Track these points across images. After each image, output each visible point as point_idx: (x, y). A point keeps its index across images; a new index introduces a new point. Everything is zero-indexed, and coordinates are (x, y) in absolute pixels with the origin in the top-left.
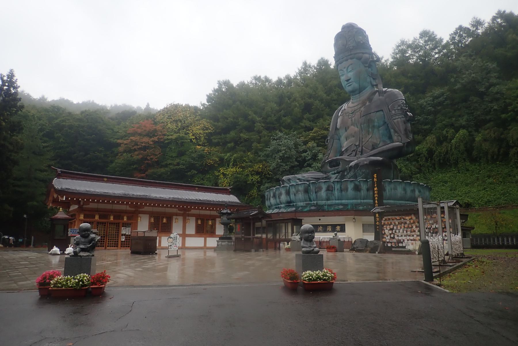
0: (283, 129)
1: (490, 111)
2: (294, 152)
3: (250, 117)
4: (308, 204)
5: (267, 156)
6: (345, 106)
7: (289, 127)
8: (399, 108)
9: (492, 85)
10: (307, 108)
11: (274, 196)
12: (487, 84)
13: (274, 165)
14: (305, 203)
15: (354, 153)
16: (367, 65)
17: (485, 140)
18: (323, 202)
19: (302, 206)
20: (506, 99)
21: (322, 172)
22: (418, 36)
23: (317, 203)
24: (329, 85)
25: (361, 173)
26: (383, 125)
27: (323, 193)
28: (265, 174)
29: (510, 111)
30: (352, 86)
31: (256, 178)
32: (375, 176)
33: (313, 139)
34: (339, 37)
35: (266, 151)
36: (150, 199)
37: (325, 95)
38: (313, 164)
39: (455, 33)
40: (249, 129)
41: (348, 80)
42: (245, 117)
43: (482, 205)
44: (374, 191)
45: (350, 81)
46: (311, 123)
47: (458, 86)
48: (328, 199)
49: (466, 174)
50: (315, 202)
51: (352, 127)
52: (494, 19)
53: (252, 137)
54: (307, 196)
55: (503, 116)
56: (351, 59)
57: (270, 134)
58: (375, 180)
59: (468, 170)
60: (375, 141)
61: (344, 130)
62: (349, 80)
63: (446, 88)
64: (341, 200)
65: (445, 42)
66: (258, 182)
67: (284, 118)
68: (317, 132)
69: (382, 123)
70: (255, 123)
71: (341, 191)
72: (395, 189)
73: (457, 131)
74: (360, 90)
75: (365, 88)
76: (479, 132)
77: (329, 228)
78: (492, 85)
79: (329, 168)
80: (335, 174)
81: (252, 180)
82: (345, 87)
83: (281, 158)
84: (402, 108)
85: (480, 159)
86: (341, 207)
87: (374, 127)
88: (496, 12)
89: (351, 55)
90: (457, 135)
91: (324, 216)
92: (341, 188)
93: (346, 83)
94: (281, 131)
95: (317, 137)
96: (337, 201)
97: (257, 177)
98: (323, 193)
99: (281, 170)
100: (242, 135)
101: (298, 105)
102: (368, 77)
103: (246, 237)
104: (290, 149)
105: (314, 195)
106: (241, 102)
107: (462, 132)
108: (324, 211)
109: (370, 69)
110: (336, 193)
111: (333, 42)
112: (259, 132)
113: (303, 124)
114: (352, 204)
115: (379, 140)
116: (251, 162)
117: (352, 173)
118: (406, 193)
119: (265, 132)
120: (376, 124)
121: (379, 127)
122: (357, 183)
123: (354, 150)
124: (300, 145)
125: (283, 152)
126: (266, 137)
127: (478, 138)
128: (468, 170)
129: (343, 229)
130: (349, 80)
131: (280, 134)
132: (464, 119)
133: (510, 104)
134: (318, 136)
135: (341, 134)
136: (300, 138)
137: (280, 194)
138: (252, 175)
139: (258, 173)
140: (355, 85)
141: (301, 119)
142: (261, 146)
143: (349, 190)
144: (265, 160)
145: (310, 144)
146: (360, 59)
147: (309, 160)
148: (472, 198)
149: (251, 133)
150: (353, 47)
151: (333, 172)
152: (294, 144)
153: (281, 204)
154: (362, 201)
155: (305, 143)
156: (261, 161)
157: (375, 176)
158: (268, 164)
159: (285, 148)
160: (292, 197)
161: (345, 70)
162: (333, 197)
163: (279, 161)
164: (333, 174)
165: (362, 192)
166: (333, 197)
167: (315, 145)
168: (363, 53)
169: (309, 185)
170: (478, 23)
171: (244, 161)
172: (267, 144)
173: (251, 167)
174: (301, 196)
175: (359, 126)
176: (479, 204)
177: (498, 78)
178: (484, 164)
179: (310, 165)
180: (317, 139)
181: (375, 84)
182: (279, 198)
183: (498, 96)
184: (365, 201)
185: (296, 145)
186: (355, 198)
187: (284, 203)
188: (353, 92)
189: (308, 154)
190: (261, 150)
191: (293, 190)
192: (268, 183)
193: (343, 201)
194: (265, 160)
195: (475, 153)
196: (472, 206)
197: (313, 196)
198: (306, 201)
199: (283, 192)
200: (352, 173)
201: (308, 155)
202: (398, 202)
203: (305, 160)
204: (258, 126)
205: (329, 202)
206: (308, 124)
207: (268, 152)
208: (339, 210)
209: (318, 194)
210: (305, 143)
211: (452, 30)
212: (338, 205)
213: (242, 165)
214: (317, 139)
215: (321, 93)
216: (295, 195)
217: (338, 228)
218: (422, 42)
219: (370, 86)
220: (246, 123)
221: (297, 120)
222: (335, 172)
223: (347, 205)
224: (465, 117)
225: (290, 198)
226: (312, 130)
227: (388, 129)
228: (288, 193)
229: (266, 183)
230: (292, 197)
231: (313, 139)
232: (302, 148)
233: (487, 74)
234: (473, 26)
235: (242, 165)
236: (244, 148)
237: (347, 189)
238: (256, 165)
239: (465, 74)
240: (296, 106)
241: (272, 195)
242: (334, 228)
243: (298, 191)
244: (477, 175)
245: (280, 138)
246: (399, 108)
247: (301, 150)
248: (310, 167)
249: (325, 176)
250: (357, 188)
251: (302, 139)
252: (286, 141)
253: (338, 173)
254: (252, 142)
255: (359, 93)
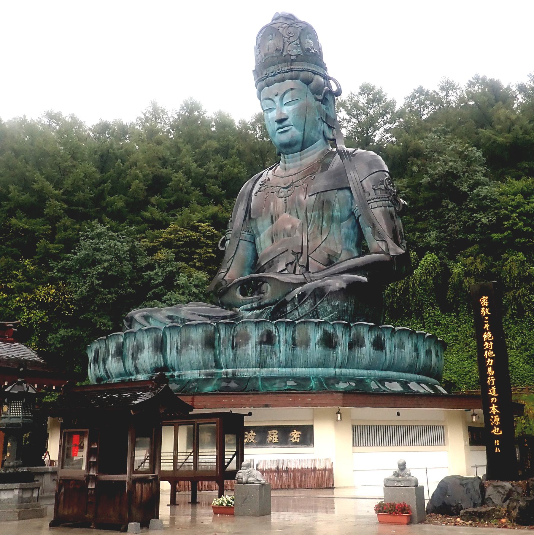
0: (107, 219)
1: (474, 226)
2: (127, 267)
3: (36, 186)
4: (212, 374)
5: (66, 271)
6: (267, 174)
7: (118, 216)
8: (382, 187)
9: (477, 184)
10: (157, 184)
11: (120, 353)
12: (471, 181)
13: (84, 289)
14: (203, 371)
15: (291, 268)
16: (320, 97)
17: (467, 274)
18: (250, 372)
19: (197, 380)
20: (499, 208)
21: (221, 305)
22: (357, 91)
23: (234, 373)
24: (203, 148)
25: (329, 308)
26: (349, 217)
27: (251, 350)
28: (60, 310)
29: (507, 229)
30: (289, 133)
31: (37, 315)
32: (484, 301)
33: (168, 244)
34: (269, 32)
35: (68, 259)
36: (38, 518)
37: (195, 165)
38: (165, 294)
39: (413, 97)
40: (34, 210)
41: (280, 121)
42: (26, 185)
43: (472, 386)
44: (481, 342)
45: (286, 123)
46: (165, 214)
47: (425, 180)
48: (261, 365)
49: (436, 330)
50: (230, 370)
51: (287, 215)
52: (471, 84)
53: (38, 227)
54: (212, 357)
55: (496, 236)
56: (291, 79)
57: (78, 226)
58: (484, 311)
59: (438, 324)
60: (333, 247)
61: (269, 221)
62: (285, 119)
63: (405, 181)
64: (291, 366)
65: (397, 108)
66: (43, 325)
67: (109, 199)
68: (176, 231)
69: (347, 213)
70: (46, 200)
71: (294, 344)
72: (401, 346)
73: (421, 255)
74: (304, 144)
75: (313, 142)
76: (456, 261)
77: (274, 436)
78: (477, 184)
79: (240, 296)
80: (252, 309)
81: (30, 319)
82: (274, 133)
83: (100, 276)
84: (386, 189)
85: (458, 306)
86: (291, 383)
87: (332, 219)
88: (473, 76)
89: (292, 70)
90: (422, 262)
91: (267, 406)
92: (293, 339)
93: (276, 125)
94: (101, 222)
95: (175, 243)
96: (283, 370)
97: (40, 314)
98: (251, 350)
99: (97, 300)
100: (14, 221)
101: (141, 175)
102: (320, 122)
103: (104, 477)
104: (120, 260)
105: (229, 352)
106: (17, 153)
107: (430, 257)
108: (255, 392)
109: (324, 107)
110: (282, 350)
111: (253, 43)
112: (54, 220)
113: (147, 214)
114: (317, 378)
115: (340, 247)
116: (29, 280)
117: (306, 308)
118: (418, 356)
119: (67, 221)
120: (336, 213)
121: (342, 221)
122: (329, 329)
123: (292, 263)
124: (140, 255)
125: (106, 264)
126: (69, 232)
127: (457, 270)
128: (438, 324)
129: (306, 436)
130: (285, 119)
131: (100, 229)
132: (433, 236)
133: (508, 218)
134: (178, 240)
135: (260, 228)
136: (140, 241)
137: (139, 348)
138: (30, 309)
139: (42, 305)
140: (295, 133)
141: (145, 204)
142: (57, 249)
143: (312, 343)
144: (64, 279)
145: (162, 255)
146: (307, 82)
147: (157, 285)
148: (454, 373)
149: (34, 221)
150: (297, 56)
151: (249, 306)
152: (129, 250)
153: (138, 372)
154: (338, 370)
155: (152, 251)
156: (53, 281)
157: (484, 301)
158: (69, 288)
159: (109, 257)
160: (171, 356)
161: (277, 99)
162: (275, 360)
163: (97, 282)
164: (247, 310)
165: (339, 349)
166: (275, 360)
167: (172, 256)
168: (314, 73)
169: (217, 330)
170: (448, 87)
171: (15, 277)
172: (70, 245)
173: (30, 290)
174: (195, 354)
175: (302, 215)
176: (466, 384)
177: (485, 175)
178: (464, 315)
179: (158, 297)
180: (176, 247)
181: (331, 137)
182: (134, 358)
183: (488, 203)
184: (344, 371)
185: (133, 253)
186: (323, 365)
187: (145, 371)
188: (288, 147)
189: (156, 274)
190: (56, 258)
191: (173, 339)
192: (64, 328)
193: (299, 371)
194: (61, 279)
195: (450, 294)
196: (455, 387)
197: (226, 355)
198: (206, 367)
199: (147, 342)
200: (306, 308)
201: (157, 275)
202: (404, 374)
203: (148, 285)
204: (55, 206)
205: (264, 372)
206: (158, 215)
207: (69, 263)
208: (289, 391)
209: (240, 352)
210: (152, 251)
211: (409, 92)
212: (285, 378)
213: (9, 285)
214: (176, 247)
215: (188, 160)
216: (179, 352)
217: (295, 435)
218: (362, 101)
219: (321, 141)
220: (25, 197)
221: (137, 205)
222: (255, 305)
223: (307, 379)
224: (434, 234)
225: (165, 358)
226: (166, 226)
227: (357, 225)
228: (160, 346)
229: (59, 327)
230: (171, 356)
231: (168, 244)
232: (143, 261)
233: (469, 165)
234: (442, 89)
235: (9, 285)
236: (15, 250)
237: (307, 343)
238: (40, 287)
239: (439, 160)
240: (136, 177)
241: (112, 349)
242: (284, 434)
243: (186, 343)
244: (455, 333)
245: (99, 236)
246: (382, 187)
247: (143, 265)
248: (160, 300)
249: (229, 313)
250: (329, 342)
251: (146, 242)
252: (112, 243)
253: (259, 307)
254: (37, 239)
255: (301, 151)
